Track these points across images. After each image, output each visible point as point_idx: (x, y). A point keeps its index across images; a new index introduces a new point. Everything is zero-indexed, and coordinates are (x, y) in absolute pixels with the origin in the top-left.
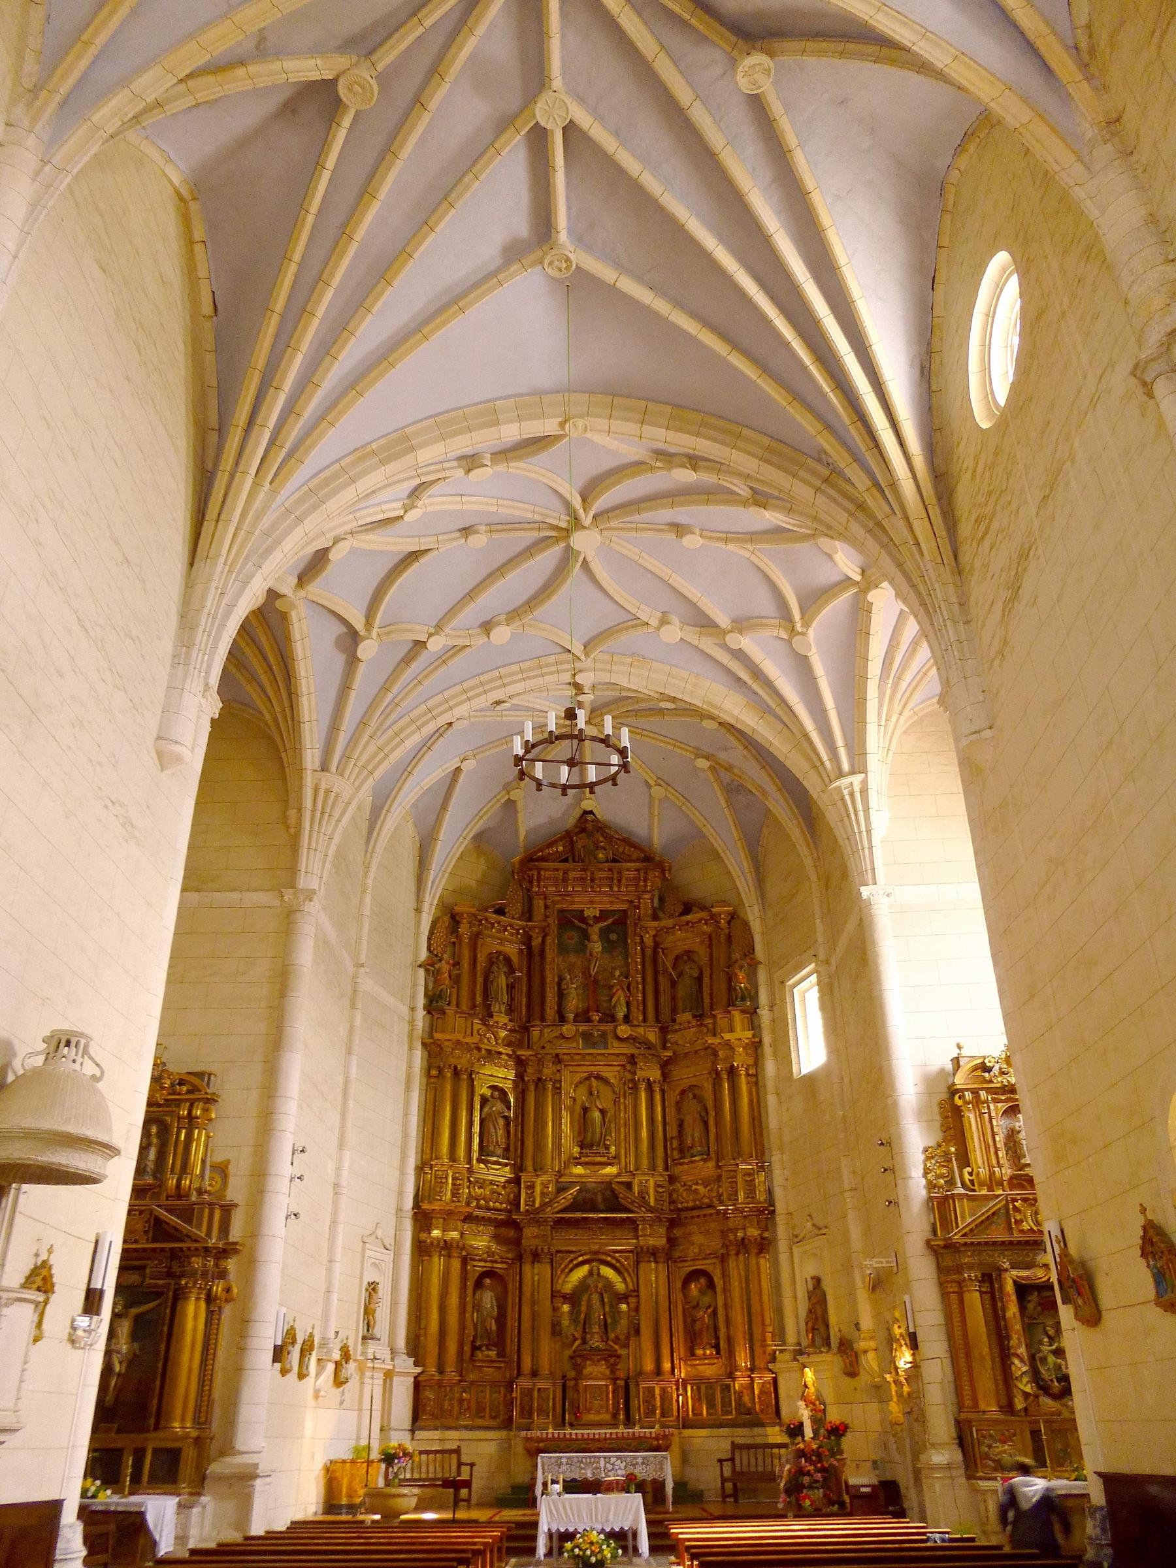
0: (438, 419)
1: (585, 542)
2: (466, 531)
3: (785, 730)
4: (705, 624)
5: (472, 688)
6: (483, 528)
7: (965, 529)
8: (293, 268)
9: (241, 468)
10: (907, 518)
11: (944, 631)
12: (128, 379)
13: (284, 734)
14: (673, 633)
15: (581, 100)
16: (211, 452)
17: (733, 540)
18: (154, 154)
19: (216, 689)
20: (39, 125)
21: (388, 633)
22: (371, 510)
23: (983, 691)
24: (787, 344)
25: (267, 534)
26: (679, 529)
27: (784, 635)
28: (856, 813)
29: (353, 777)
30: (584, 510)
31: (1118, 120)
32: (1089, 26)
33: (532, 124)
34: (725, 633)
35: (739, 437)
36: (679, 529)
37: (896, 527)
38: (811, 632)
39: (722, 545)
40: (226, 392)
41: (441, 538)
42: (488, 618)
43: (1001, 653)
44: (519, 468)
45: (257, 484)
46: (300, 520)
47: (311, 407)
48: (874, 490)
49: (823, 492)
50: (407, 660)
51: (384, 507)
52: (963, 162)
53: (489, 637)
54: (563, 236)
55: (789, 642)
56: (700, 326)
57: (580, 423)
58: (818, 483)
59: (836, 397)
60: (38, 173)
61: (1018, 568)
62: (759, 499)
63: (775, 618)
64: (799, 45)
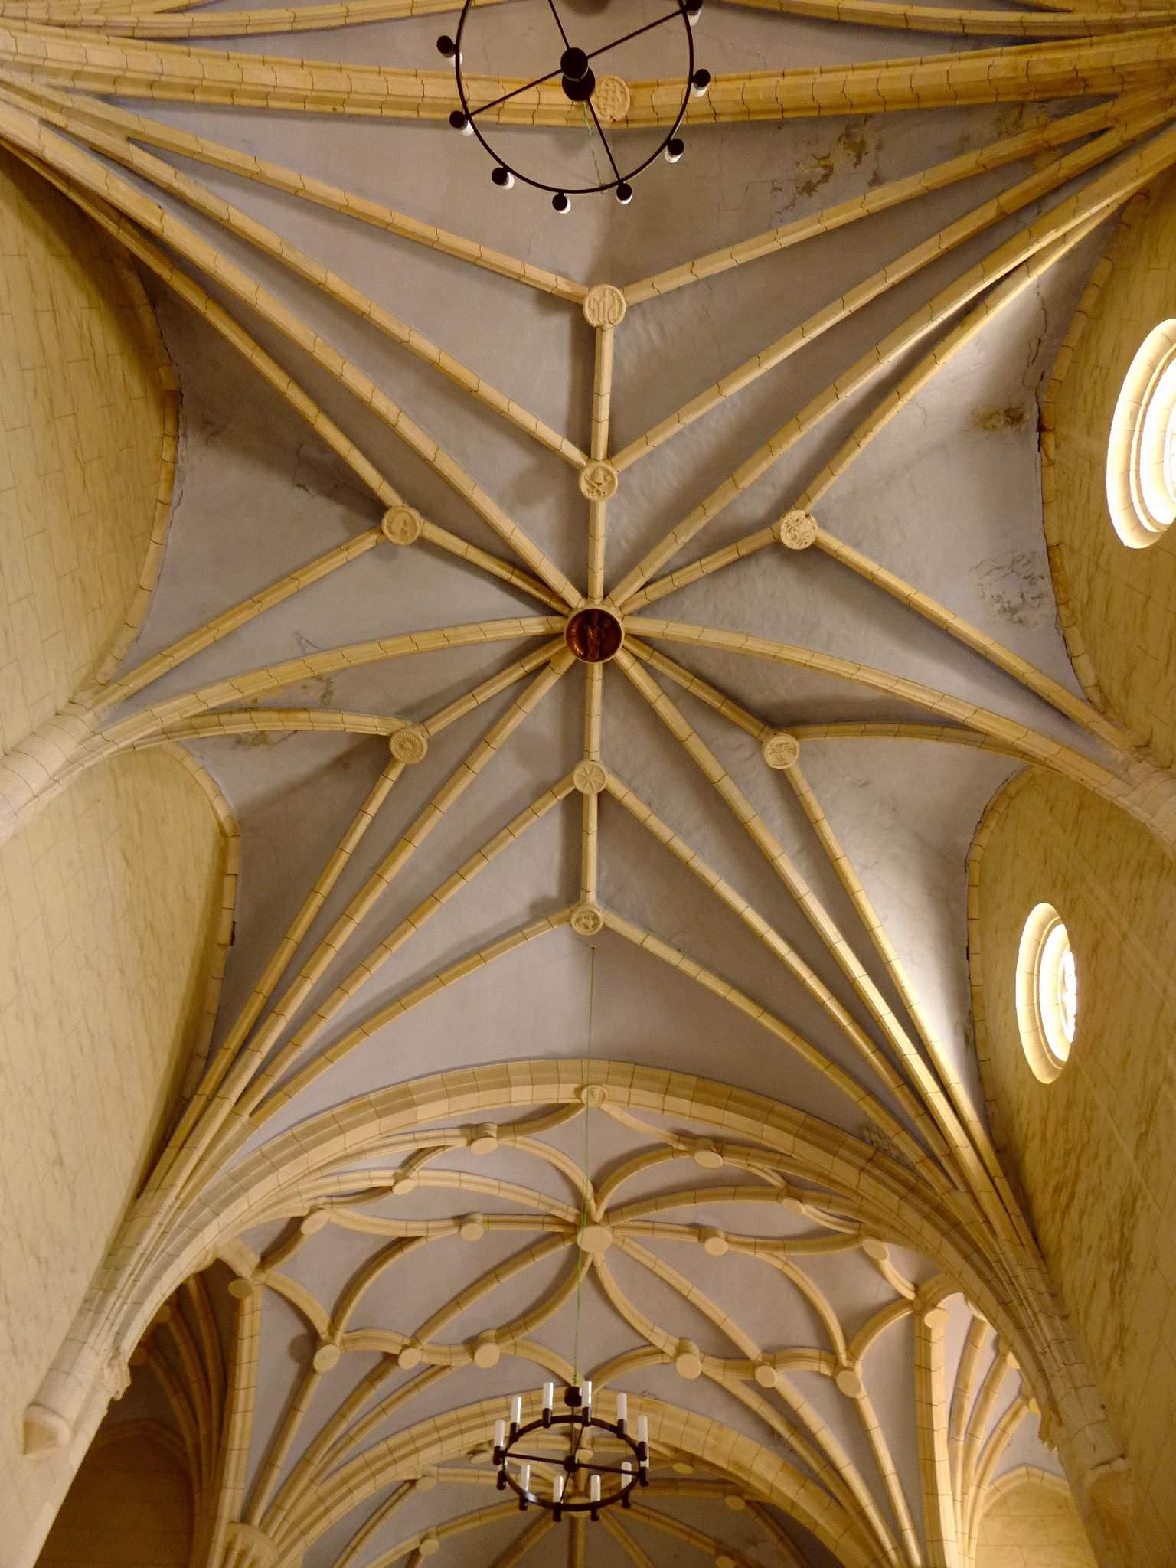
0: (445, 1075)
1: (595, 1241)
2: (461, 1220)
3: (834, 1505)
4: (729, 1353)
5: (446, 1426)
6: (480, 1218)
7: (1042, 1204)
8: (318, 901)
9: (222, 1092)
10: (971, 1192)
11: (1037, 1327)
12: (122, 972)
13: (204, 1469)
14: (692, 1365)
15: (617, 774)
16: (193, 1078)
17: (763, 1247)
18: (207, 785)
19: (127, 1359)
20: (99, 708)
21: (354, 1340)
22: (357, 1175)
23: (1103, 1407)
24: (821, 1005)
25: (234, 1178)
26: (701, 1232)
27: (827, 1371)
29: (278, 1537)
30: (596, 1201)
31: (1147, 745)
32: (1098, 686)
33: (571, 789)
34: (755, 1366)
35: (771, 1111)
36: (701, 1232)
37: (959, 1204)
38: (859, 1368)
39: (750, 1252)
40: (223, 1022)
41: (431, 1225)
43: (1119, 1346)
44: (525, 1143)
45: (235, 1113)
46: (275, 1167)
47: (310, 1041)
48: (928, 1161)
49: (868, 1172)
50: (374, 1377)
51: (373, 1174)
52: (984, 839)
53: (473, 1357)
54: (592, 897)
55: (833, 1380)
56: (729, 988)
57: (598, 1090)
58: (862, 1163)
59: (878, 1058)
60: (84, 740)
61: (1122, 1229)
62: (795, 1190)
63: (816, 1348)
64: (824, 728)
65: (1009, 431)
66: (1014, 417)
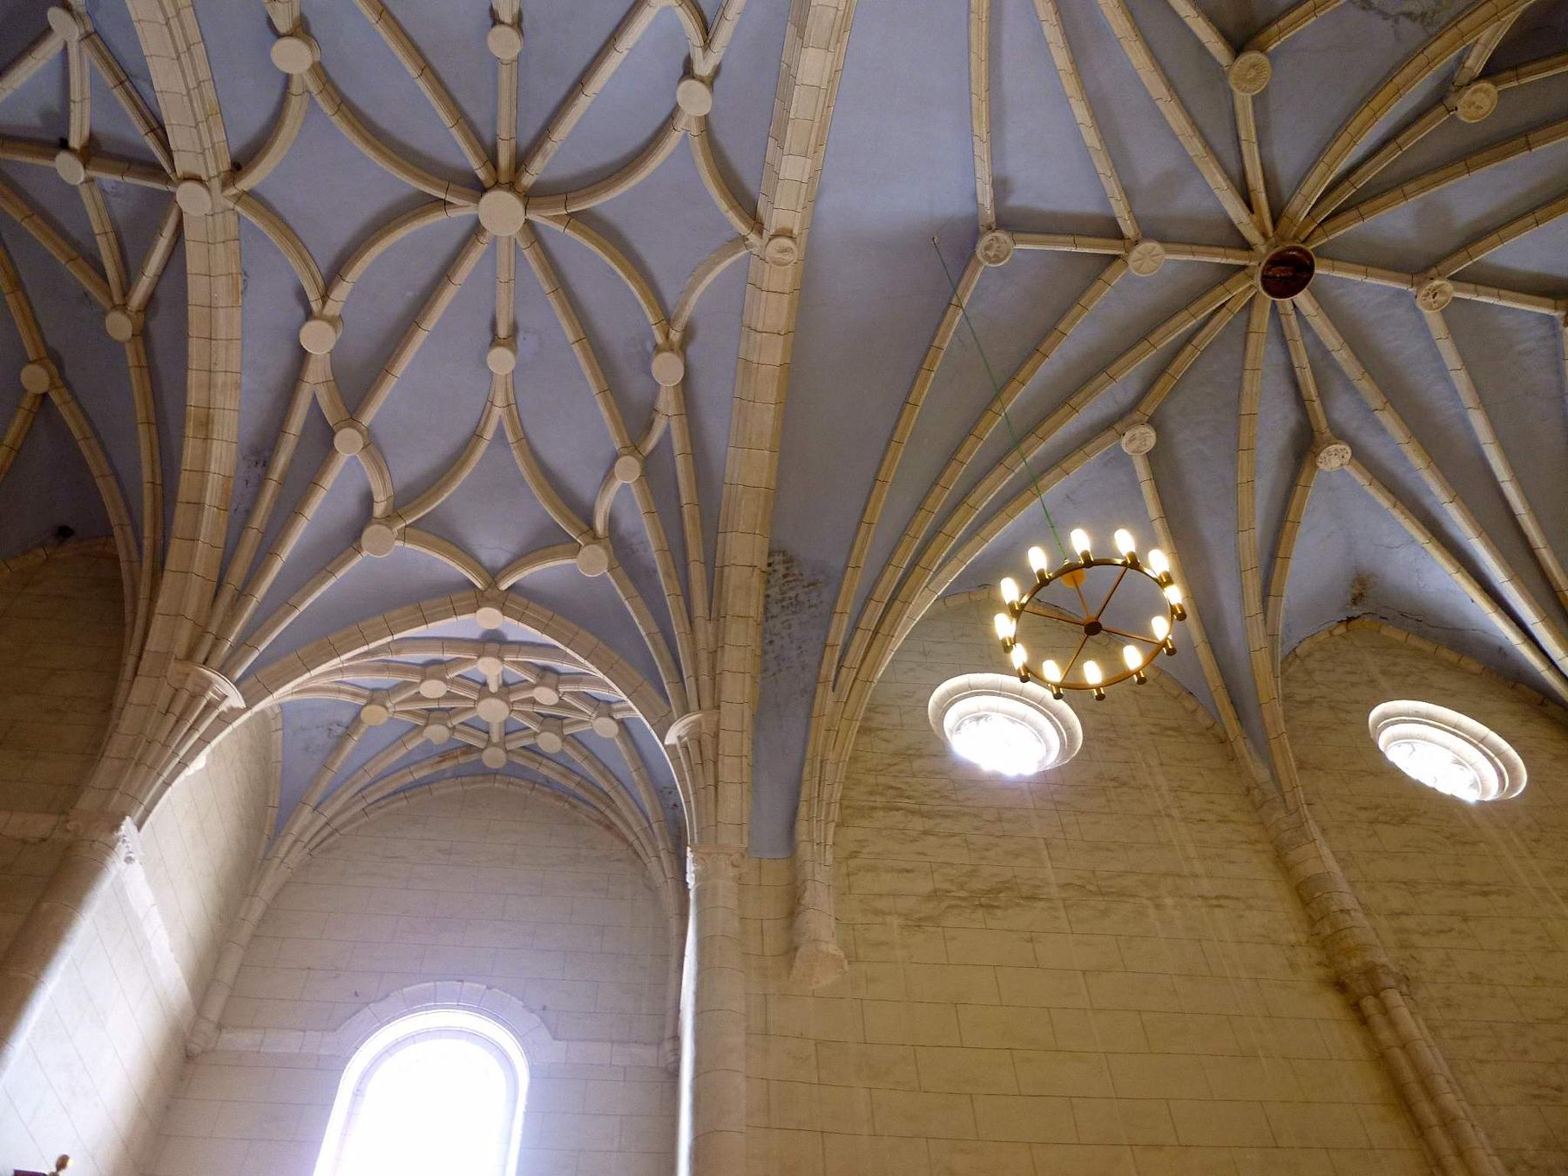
28: (192, 728)
42: (314, 30)
65: (1349, 598)
66: (1357, 599)
